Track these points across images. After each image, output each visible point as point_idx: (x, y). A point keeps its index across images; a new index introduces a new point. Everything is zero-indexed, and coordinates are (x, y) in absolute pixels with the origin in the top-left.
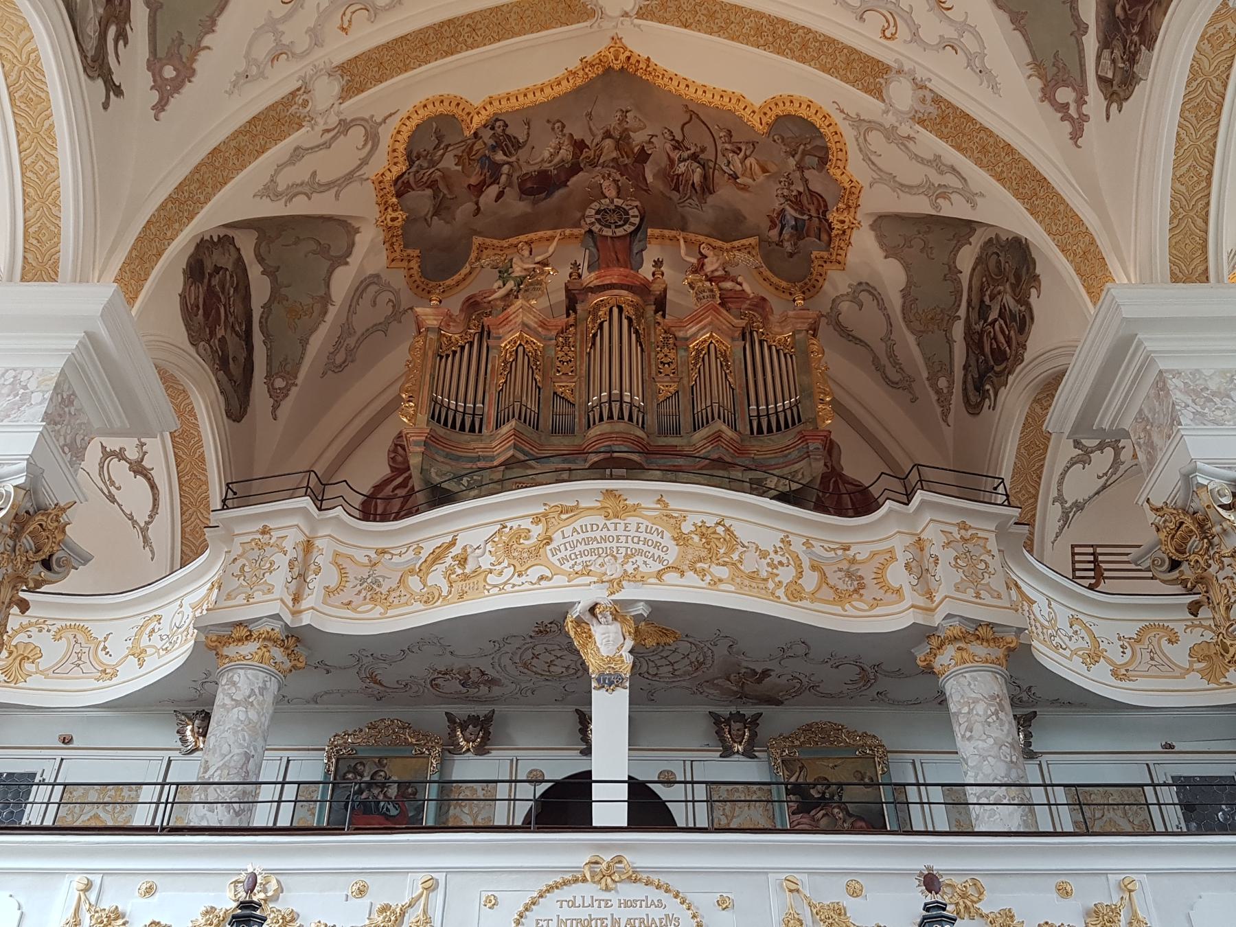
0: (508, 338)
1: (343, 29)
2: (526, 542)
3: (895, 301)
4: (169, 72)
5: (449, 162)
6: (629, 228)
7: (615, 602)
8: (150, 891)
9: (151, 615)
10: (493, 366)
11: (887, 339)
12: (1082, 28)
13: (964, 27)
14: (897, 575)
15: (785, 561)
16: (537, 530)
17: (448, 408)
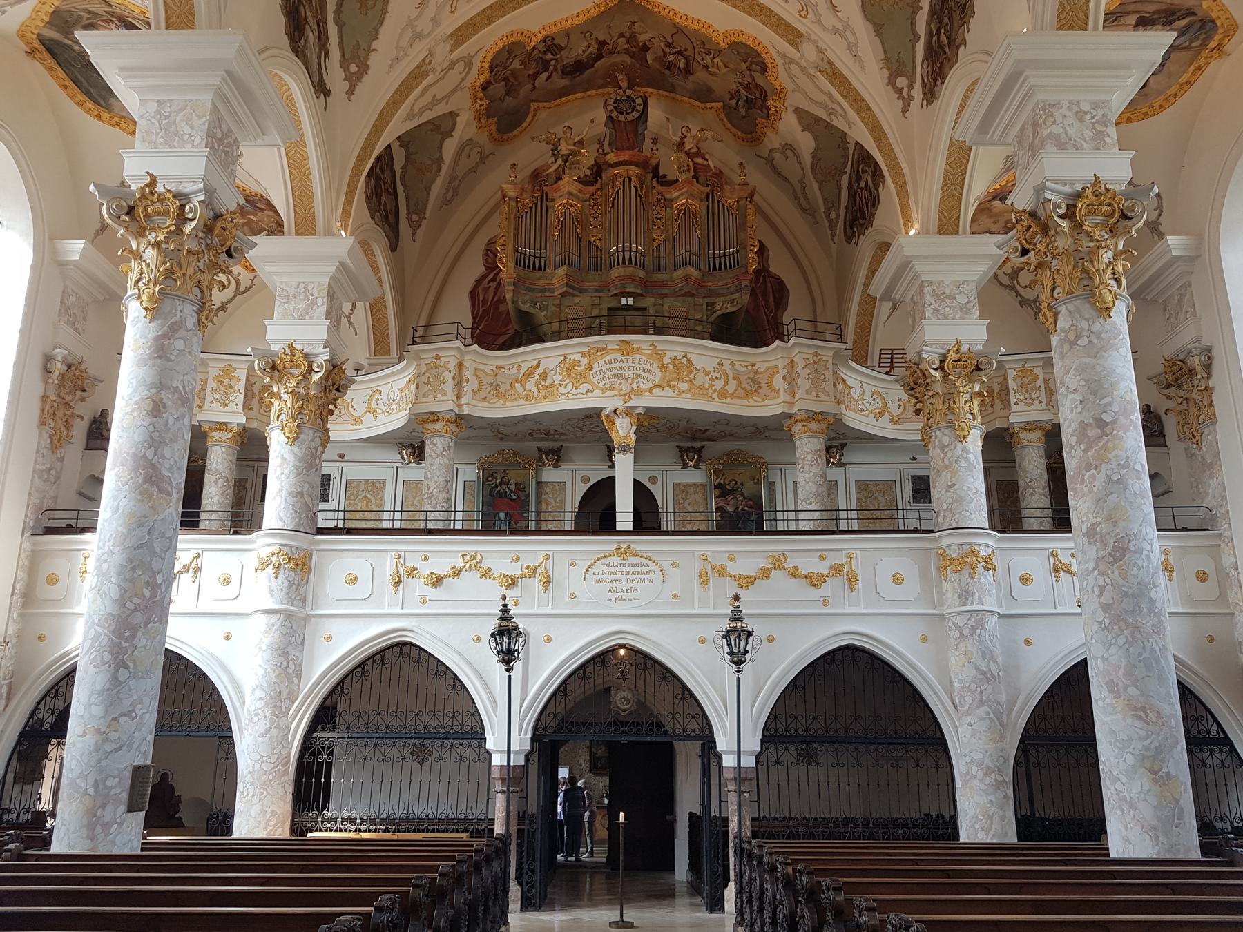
0: (560, 203)
1: (452, 12)
2: (579, 369)
3: (807, 160)
4: (353, 68)
5: (516, 65)
6: (636, 114)
7: (627, 407)
8: (426, 558)
9: (375, 389)
10: (551, 221)
11: (802, 181)
12: (916, 37)
13: (847, 26)
14: (778, 382)
15: (719, 376)
16: (584, 361)
17: (525, 254)
